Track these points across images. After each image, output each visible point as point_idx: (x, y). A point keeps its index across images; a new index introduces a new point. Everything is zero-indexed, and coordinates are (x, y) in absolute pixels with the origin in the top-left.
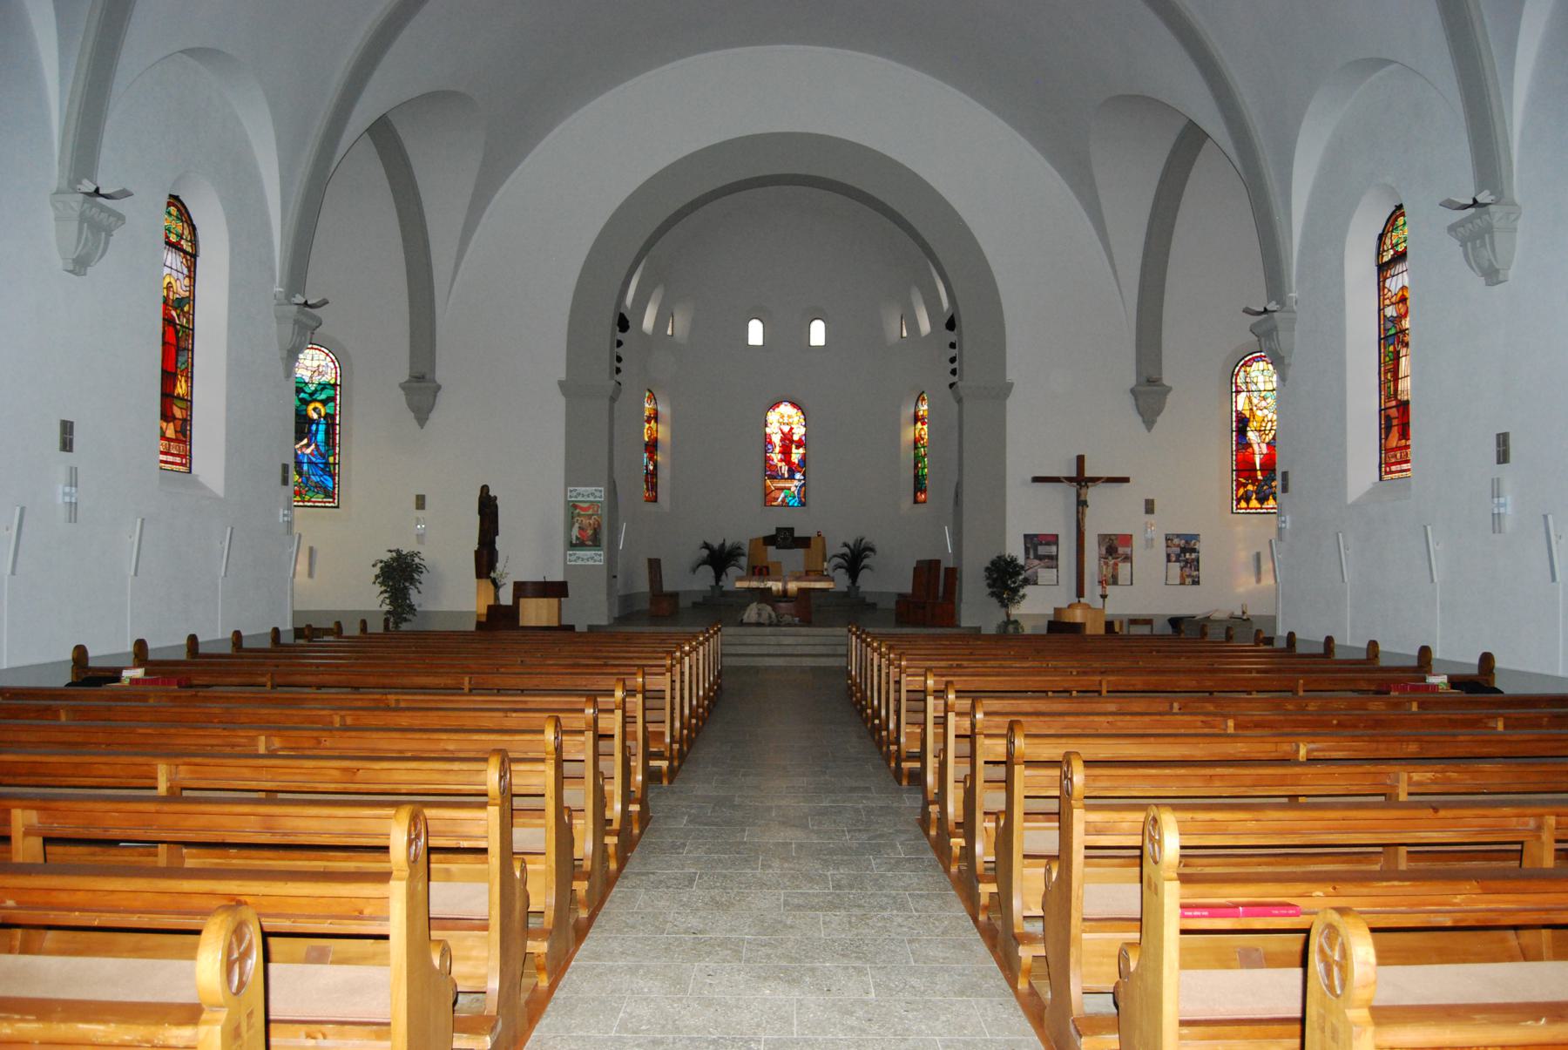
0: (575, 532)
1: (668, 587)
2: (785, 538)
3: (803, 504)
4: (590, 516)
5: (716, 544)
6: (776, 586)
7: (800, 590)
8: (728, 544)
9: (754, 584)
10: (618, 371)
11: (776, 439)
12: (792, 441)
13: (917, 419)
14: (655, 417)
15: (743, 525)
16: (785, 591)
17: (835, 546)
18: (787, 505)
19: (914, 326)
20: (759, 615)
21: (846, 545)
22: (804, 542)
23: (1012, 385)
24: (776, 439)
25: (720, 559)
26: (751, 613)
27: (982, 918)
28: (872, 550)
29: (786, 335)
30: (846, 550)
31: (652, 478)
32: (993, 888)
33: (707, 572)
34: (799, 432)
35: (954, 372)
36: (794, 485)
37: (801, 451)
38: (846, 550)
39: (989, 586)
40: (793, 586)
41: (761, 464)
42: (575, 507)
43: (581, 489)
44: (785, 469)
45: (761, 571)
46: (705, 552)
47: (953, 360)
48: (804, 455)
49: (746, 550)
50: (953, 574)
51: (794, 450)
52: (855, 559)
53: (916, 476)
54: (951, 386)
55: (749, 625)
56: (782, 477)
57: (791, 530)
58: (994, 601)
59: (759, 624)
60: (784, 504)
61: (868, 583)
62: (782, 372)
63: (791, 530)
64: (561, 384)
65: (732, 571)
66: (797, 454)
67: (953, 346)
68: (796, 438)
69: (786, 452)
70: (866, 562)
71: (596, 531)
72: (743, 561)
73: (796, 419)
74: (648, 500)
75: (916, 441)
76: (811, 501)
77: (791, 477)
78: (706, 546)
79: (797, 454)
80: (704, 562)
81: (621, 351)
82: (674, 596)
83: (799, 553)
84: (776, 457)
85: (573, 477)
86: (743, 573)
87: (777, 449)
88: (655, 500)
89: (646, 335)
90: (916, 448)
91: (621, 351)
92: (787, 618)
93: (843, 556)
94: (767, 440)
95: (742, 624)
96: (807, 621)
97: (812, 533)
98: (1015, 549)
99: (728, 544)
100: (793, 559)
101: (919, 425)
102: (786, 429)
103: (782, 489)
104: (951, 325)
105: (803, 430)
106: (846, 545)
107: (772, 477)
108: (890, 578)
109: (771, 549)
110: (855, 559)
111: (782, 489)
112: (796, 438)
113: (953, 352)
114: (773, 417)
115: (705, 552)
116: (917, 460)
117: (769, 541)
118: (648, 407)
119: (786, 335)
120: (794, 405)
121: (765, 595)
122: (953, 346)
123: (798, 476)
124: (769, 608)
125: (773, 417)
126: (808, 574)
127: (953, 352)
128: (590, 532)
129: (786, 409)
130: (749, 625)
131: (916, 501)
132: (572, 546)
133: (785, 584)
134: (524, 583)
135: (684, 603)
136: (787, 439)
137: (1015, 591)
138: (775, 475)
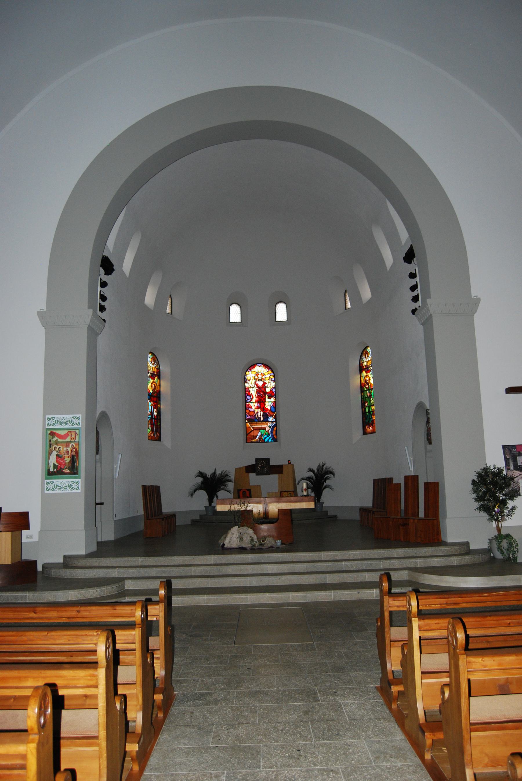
0: (53, 460)
1: (166, 509)
2: (262, 467)
3: (275, 440)
4: (67, 444)
5: (209, 473)
6: (257, 508)
7: (281, 511)
8: (218, 472)
9: (235, 507)
10: (102, 309)
11: (253, 391)
12: (265, 393)
13: (362, 369)
14: (157, 374)
15: (230, 457)
16: (266, 513)
17: (302, 471)
18: (263, 441)
19: (356, 298)
20: (241, 539)
21: (311, 470)
22: (278, 469)
23: (477, 301)
24: (253, 391)
25: (212, 484)
26: (233, 537)
27: (428, 756)
28: (332, 473)
29: (258, 313)
30: (311, 474)
31: (156, 423)
32: (401, 688)
33: (202, 495)
34: (270, 386)
35: (415, 299)
36: (268, 426)
37: (273, 400)
38: (311, 474)
39: (476, 500)
40: (274, 508)
41: (241, 408)
42: (53, 434)
43: (59, 417)
44: (260, 414)
45: (245, 493)
46: (200, 480)
47: (414, 288)
48: (275, 402)
49: (233, 477)
50: (433, 490)
51: (267, 400)
52: (319, 480)
53: (364, 413)
54: (414, 311)
55: (231, 551)
56: (259, 420)
57: (267, 460)
58: (484, 515)
59: (241, 550)
60: (261, 440)
61: (330, 499)
62: (259, 343)
63: (267, 460)
64: (41, 315)
65: (221, 494)
66: (269, 403)
67: (412, 276)
68: (268, 390)
69: (261, 401)
70: (328, 482)
71: (74, 459)
72: (231, 486)
73: (268, 376)
74: (152, 439)
75: (362, 386)
76: (282, 436)
77: (266, 420)
78: (201, 474)
79: (269, 403)
80: (200, 488)
81: (106, 291)
82: (172, 516)
83: (274, 478)
84: (254, 405)
85: (50, 406)
86: (231, 496)
87: (254, 399)
88: (159, 439)
89: (145, 307)
90: (362, 391)
91: (106, 291)
92: (269, 542)
93: (309, 479)
94: (246, 392)
95: (224, 550)
96: (290, 546)
97: (285, 463)
98: (496, 460)
99: (218, 472)
100: (270, 482)
101: (364, 373)
102: (260, 384)
103: (259, 429)
104: (409, 257)
105: (273, 384)
106: (311, 470)
107: (251, 421)
108: (349, 494)
109: (252, 476)
110: (319, 480)
111: (259, 429)
112: (268, 390)
113: (413, 282)
114: (250, 375)
115: (200, 480)
116: (364, 400)
117: (250, 469)
118: (151, 366)
119: (258, 313)
120: (266, 366)
121: (245, 519)
122: (412, 276)
123: (271, 419)
124: (251, 531)
125: (250, 375)
126: (281, 496)
127: (413, 282)
128: (68, 460)
129: (260, 369)
130: (231, 551)
131: (365, 433)
132: (50, 474)
133: (266, 504)
134: (378, 480)
135: (179, 522)
136: (261, 391)
137: (504, 503)
138: (253, 419)
